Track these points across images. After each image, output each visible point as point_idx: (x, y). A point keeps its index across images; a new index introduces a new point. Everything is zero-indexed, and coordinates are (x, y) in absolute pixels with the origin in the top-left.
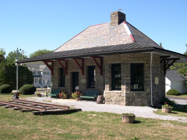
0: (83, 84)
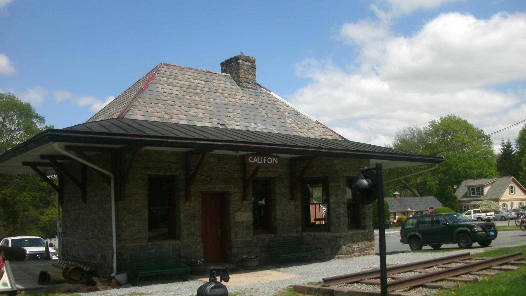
0: (245, 225)
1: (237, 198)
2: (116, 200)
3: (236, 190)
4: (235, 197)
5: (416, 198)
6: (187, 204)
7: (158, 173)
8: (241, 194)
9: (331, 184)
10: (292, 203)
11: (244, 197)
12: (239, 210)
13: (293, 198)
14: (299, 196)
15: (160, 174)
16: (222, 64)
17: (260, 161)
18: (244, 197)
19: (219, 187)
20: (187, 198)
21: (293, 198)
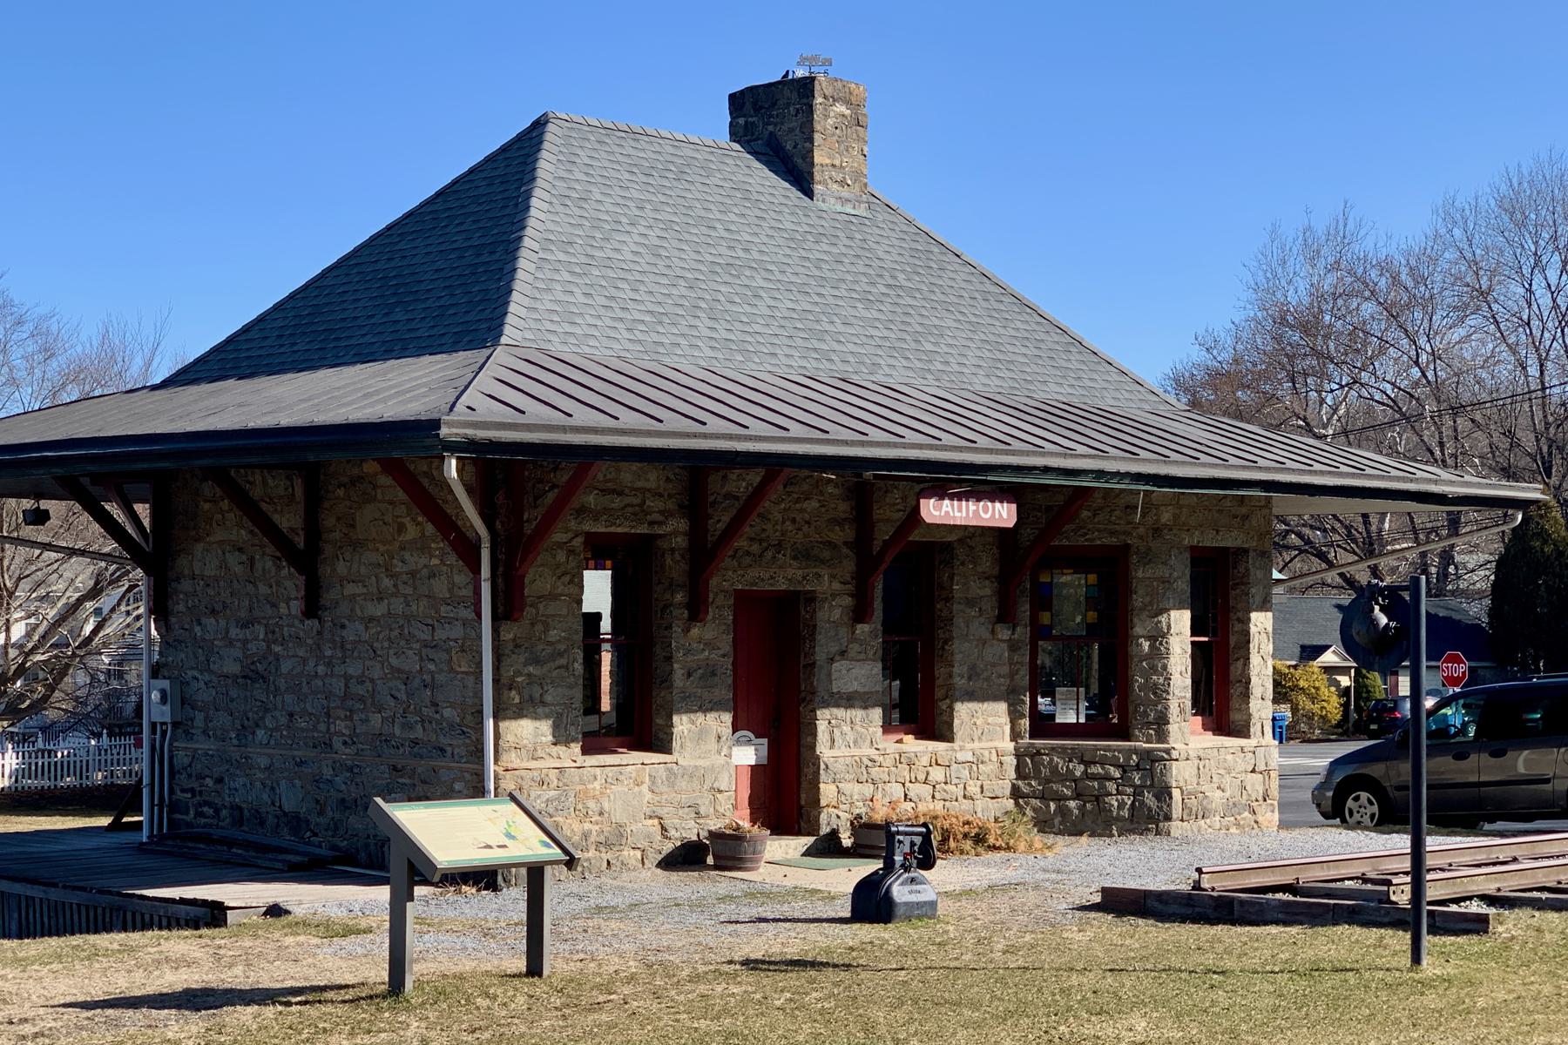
1: (837, 614)
2: (495, 618)
3: (836, 586)
4: (832, 613)
5: (993, 386)
6: (695, 632)
7: (612, 529)
8: (848, 601)
9: (1140, 574)
10: (1004, 633)
11: (860, 613)
12: (843, 653)
13: (1005, 616)
14: (1024, 610)
15: (619, 530)
16: (739, 102)
17: (960, 510)
18: (860, 613)
19: (783, 577)
20: (697, 610)
21: (1005, 616)
